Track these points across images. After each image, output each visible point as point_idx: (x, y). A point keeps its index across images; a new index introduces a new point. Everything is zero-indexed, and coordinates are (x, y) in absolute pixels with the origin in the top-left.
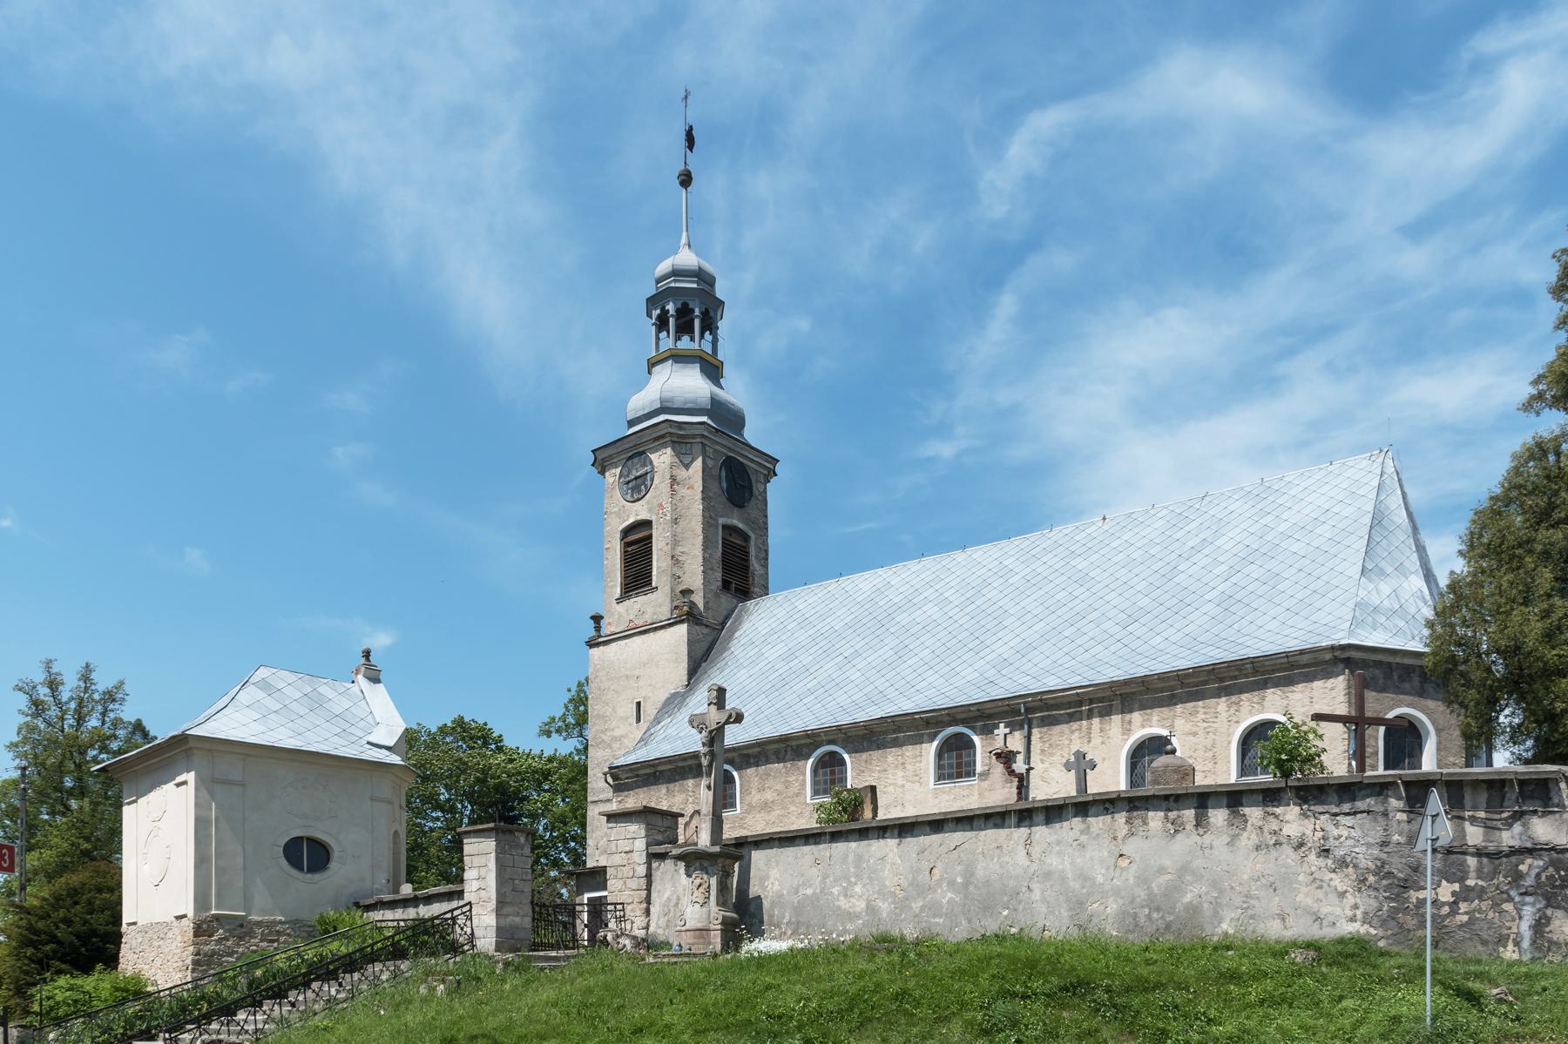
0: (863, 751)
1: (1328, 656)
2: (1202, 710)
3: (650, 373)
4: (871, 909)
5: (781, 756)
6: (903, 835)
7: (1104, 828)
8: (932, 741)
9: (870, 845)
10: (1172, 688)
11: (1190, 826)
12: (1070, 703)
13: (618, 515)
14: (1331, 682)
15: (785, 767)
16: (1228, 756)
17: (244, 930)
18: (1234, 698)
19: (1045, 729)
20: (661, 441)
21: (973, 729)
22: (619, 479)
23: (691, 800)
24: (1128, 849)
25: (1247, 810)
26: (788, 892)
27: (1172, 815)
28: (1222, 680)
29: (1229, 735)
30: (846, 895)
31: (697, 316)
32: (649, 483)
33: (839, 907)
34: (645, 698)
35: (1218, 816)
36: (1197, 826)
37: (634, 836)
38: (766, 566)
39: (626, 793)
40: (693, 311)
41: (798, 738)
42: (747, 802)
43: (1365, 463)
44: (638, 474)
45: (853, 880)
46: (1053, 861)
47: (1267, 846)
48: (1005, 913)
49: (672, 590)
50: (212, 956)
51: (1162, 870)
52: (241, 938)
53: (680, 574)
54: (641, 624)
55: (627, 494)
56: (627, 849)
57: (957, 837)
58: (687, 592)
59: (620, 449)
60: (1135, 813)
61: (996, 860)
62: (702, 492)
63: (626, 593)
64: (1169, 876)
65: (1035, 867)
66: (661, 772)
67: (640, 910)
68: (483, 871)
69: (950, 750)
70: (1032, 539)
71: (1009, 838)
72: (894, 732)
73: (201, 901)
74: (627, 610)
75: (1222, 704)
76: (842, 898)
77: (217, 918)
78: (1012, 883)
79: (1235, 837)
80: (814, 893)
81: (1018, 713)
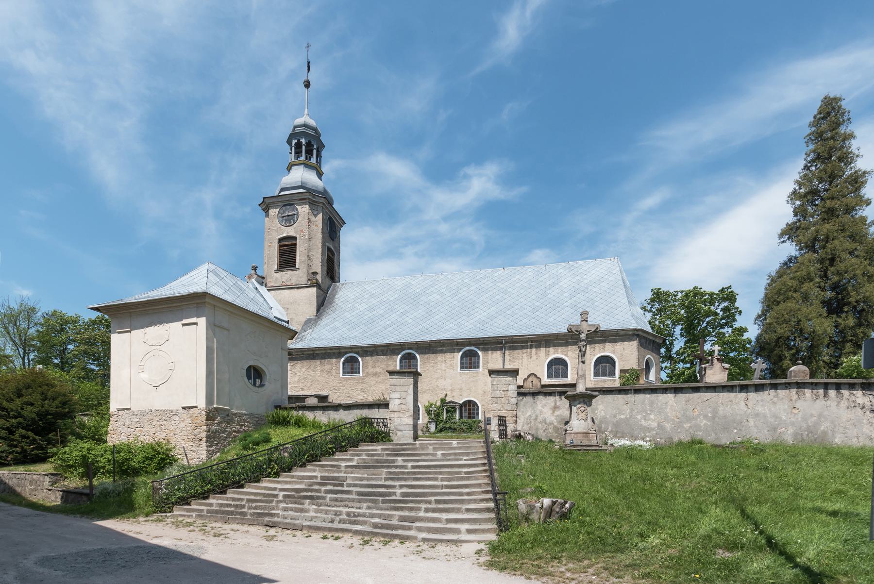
0: (426, 353)
1: (631, 333)
3: (289, 169)
4: (660, 426)
5: (385, 353)
7: (786, 395)
8: (459, 352)
10: (567, 339)
11: (822, 397)
14: (631, 343)
16: (590, 368)
17: (229, 418)
18: (592, 346)
19: (511, 351)
21: (478, 348)
23: (334, 368)
24: (797, 405)
25: (843, 391)
26: (610, 416)
27: (815, 391)
30: (645, 420)
32: (295, 219)
33: (641, 425)
34: (291, 319)
35: (832, 393)
36: (825, 396)
37: (509, 383)
38: (339, 269)
39: (296, 362)
40: (313, 146)
43: (609, 262)
44: (290, 214)
45: (649, 412)
46: (759, 409)
47: (851, 407)
48: (735, 431)
49: (308, 271)
50: (215, 433)
51: (812, 415)
52: (228, 423)
56: (505, 389)
58: (315, 273)
59: (280, 200)
60: (800, 390)
61: (729, 407)
64: (815, 418)
65: (750, 411)
68: (404, 395)
71: (736, 397)
72: (441, 346)
73: (209, 399)
77: (216, 409)
78: (738, 418)
79: (839, 403)
80: (626, 418)
81: (502, 343)
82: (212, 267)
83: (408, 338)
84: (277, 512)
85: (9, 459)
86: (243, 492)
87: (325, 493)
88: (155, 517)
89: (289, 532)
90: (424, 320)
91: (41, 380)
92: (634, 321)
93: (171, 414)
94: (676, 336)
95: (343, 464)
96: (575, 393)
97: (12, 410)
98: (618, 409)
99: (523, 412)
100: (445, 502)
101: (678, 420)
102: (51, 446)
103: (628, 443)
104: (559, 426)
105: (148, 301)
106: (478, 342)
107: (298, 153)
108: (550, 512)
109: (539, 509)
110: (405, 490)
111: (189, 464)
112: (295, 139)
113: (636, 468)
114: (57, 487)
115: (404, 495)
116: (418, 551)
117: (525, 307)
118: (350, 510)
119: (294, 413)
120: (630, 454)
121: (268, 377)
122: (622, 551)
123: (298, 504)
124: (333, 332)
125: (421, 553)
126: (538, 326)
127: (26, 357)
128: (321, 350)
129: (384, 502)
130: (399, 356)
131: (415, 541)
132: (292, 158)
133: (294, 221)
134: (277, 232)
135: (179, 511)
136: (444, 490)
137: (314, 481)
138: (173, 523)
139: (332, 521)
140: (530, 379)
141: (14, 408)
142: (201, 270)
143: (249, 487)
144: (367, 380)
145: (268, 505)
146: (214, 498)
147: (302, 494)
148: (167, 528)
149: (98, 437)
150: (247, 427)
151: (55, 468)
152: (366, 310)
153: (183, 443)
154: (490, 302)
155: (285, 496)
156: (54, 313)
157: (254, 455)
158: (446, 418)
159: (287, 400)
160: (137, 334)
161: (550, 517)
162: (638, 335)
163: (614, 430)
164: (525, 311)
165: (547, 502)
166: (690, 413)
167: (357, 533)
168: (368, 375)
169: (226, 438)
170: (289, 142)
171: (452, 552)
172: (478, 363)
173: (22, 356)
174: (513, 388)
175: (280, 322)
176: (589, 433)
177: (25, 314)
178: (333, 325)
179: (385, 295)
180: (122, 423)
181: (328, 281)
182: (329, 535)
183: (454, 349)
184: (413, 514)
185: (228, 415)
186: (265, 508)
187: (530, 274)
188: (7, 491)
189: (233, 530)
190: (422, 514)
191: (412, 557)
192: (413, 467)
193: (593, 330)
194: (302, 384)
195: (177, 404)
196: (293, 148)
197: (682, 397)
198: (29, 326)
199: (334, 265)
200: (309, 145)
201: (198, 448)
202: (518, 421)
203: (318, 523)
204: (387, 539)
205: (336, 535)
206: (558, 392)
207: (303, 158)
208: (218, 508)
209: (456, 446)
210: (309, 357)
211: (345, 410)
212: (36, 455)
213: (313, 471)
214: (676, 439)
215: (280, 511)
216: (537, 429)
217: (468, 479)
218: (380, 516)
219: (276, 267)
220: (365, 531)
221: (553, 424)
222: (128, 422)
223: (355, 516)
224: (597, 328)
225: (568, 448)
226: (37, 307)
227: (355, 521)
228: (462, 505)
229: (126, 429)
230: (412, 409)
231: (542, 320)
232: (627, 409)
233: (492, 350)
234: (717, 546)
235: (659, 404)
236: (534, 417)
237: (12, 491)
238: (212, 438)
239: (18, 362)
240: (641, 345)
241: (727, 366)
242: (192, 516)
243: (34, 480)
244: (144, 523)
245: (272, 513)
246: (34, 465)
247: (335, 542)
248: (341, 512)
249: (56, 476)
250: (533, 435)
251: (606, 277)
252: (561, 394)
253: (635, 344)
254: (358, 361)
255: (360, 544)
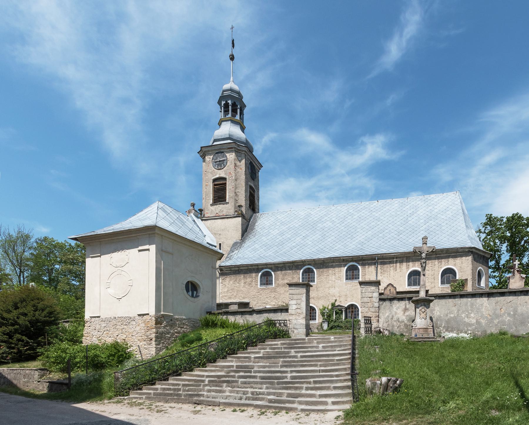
0: (321, 268)
1: (467, 250)
2: (430, 263)
3: (220, 124)
4: (478, 322)
5: (291, 268)
6: (489, 296)
8: (345, 267)
9: (476, 300)
12: (390, 258)
13: (211, 173)
14: (467, 258)
15: (292, 272)
17: (172, 322)
18: (440, 260)
19: (382, 266)
20: (231, 150)
21: (358, 264)
22: (212, 160)
23: (254, 281)
28: (436, 254)
29: (438, 272)
30: (468, 317)
31: (239, 108)
32: (225, 164)
33: (465, 322)
34: (223, 242)
37: (373, 291)
38: (258, 202)
39: (226, 276)
41: (298, 262)
42: (277, 283)
43: (453, 195)
44: (221, 160)
45: (470, 312)
49: (235, 205)
50: (162, 334)
53: (237, 199)
54: (221, 215)
55: (215, 166)
56: (370, 296)
57: (511, 298)
58: (240, 206)
59: (213, 149)
62: (245, 171)
63: (214, 203)
66: (241, 270)
67: (376, 320)
68: (299, 301)
69: (306, 273)
70: (356, 205)
72: (332, 263)
73: (158, 309)
74: (215, 209)
75: (436, 262)
76: (466, 318)
77: (163, 316)
80: (454, 316)
81: (375, 259)
82: (161, 205)
83: (308, 256)
84: (203, 393)
85: (8, 358)
86: (181, 379)
87: (238, 378)
88: (115, 400)
89: (210, 407)
90: (320, 242)
91: (33, 294)
92: (469, 241)
93: (129, 320)
94: (502, 252)
95: (253, 356)
96: (418, 298)
97: (10, 319)
98: (449, 310)
99: (383, 313)
100: (320, 382)
101: (490, 318)
102: (40, 347)
103: (455, 335)
104: (408, 323)
105: (113, 232)
106: (359, 259)
107: (226, 111)
108: (386, 387)
109: (379, 385)
110: (294, 374)
111: (142, 359)
112: (223, 101)
113: (453, 355)
114: (44, 379)
115: (293, 378)
116: (297, 418)
117: (392, 231)
118: (254, 390)
119: (220, 317)
120: (453, 344)
121: (201, 290)
122: (428, 413)
123: (218, 387)
124: (253, 252)
125: (298, 419)
126: (401, 246)
127: (22, 276)
128: (244, 267)
129: (278, 383)
130: (302, 271)
131: (296, 411)
132: (221, 115)
133: (224, 165)
134: (212, 174)
135: (133, 394)
136: (321, 374)
137: (232, 369)
138: (128, 403)
139: (241, 399)
140: (389, 288)
141: (12, 318)
142: (153, 207)
143: (185, 375)
144: (278, 289)
145: (197, 388)
146: (159, 384)
147: (222, 379)
148: (124, 407)
149: (75, 340)
150: (186, 329)
151: (43, 365)
152: (278, 235)
153: (139, 342)
154: (367, 227)
155: (209, 381)
156: (45, 239)
157: (189, 351)
158: (336, 318)
159: (216, 307)
160: (105, 258)
161: (387, 391)
162: (472, 252)
163: (446, 326)
164: (392, 234)
165: (384, 379)
166: (498, 312)
167: (257, 406)
168: (278, 285)
169: (170, 337)
170: (219, 103)
171: (320, 418)
172: (359, 275)
173: (18, 275)
174: (376, 295)
175: (211, 247)
176: (428, 329)
177: (21, 241)
178: (253, 247)
179: (292, 223)
180: (94, 328)
181: (250, 212)
182: (238, 409)
183: (341, 264)
184: (298, 392)
185: (171, 320)
186: (195, 391)
187: (397, 205)
188: (6, 383)
189: (171, 407)
190: (304, 392)
191: (292, 423)
192: (302, 357)
193: (431, 250)
194: (231, 294)
195: (133, 314)
196: (222, 108)
197: (493, 300)
198: (24, 250)
199: (254, 199)
200: (234, 105)
201: (149, 346)
202: (380, 320)
203: (231, 401)
204: (277, 411)
205: (243, 408)
206: (407, 298)
207: (230, 115)
208: (161, 392)
209: (333, 340)
210: (235, 272)
211: (257, 314)
212: (29, 354)
213: (232, 362)
214: (489, 332)
215: (205, 393)
216: (393, 326)
217: (338, 364)
218: (274, 394)
219: (211, 201)
220: (262, 405)
221: (404, 322)
222: (98, 327)
223: (257, 394)
224: (433, 249)
225: (413, 340)
226: (31, 234)
227: (256, 398)
228: (331, 384)
229: (97, 332)
230: (305, 312)
231: (404, 241)
232: (455, 309)
233: (368, 265)
234: (491, 408)
235: (477, 305)
236: (391, 317)
237: (10, 383)
238: (159, 338)
239: (15, 281)
240: (475, 259)
241: (524, 276)
242: (142, 398)
243: (27, 374)
244: (108, 404)
245: (199, 394)
246: (27, 363)
247: (241, 414)
248: (247, 392)
249: (44, 370)
250: (389, 331)
251: (450, 207)
252: (410, 299)
253: (470, 258)
254: (271, 275)
255: (258, 415)
